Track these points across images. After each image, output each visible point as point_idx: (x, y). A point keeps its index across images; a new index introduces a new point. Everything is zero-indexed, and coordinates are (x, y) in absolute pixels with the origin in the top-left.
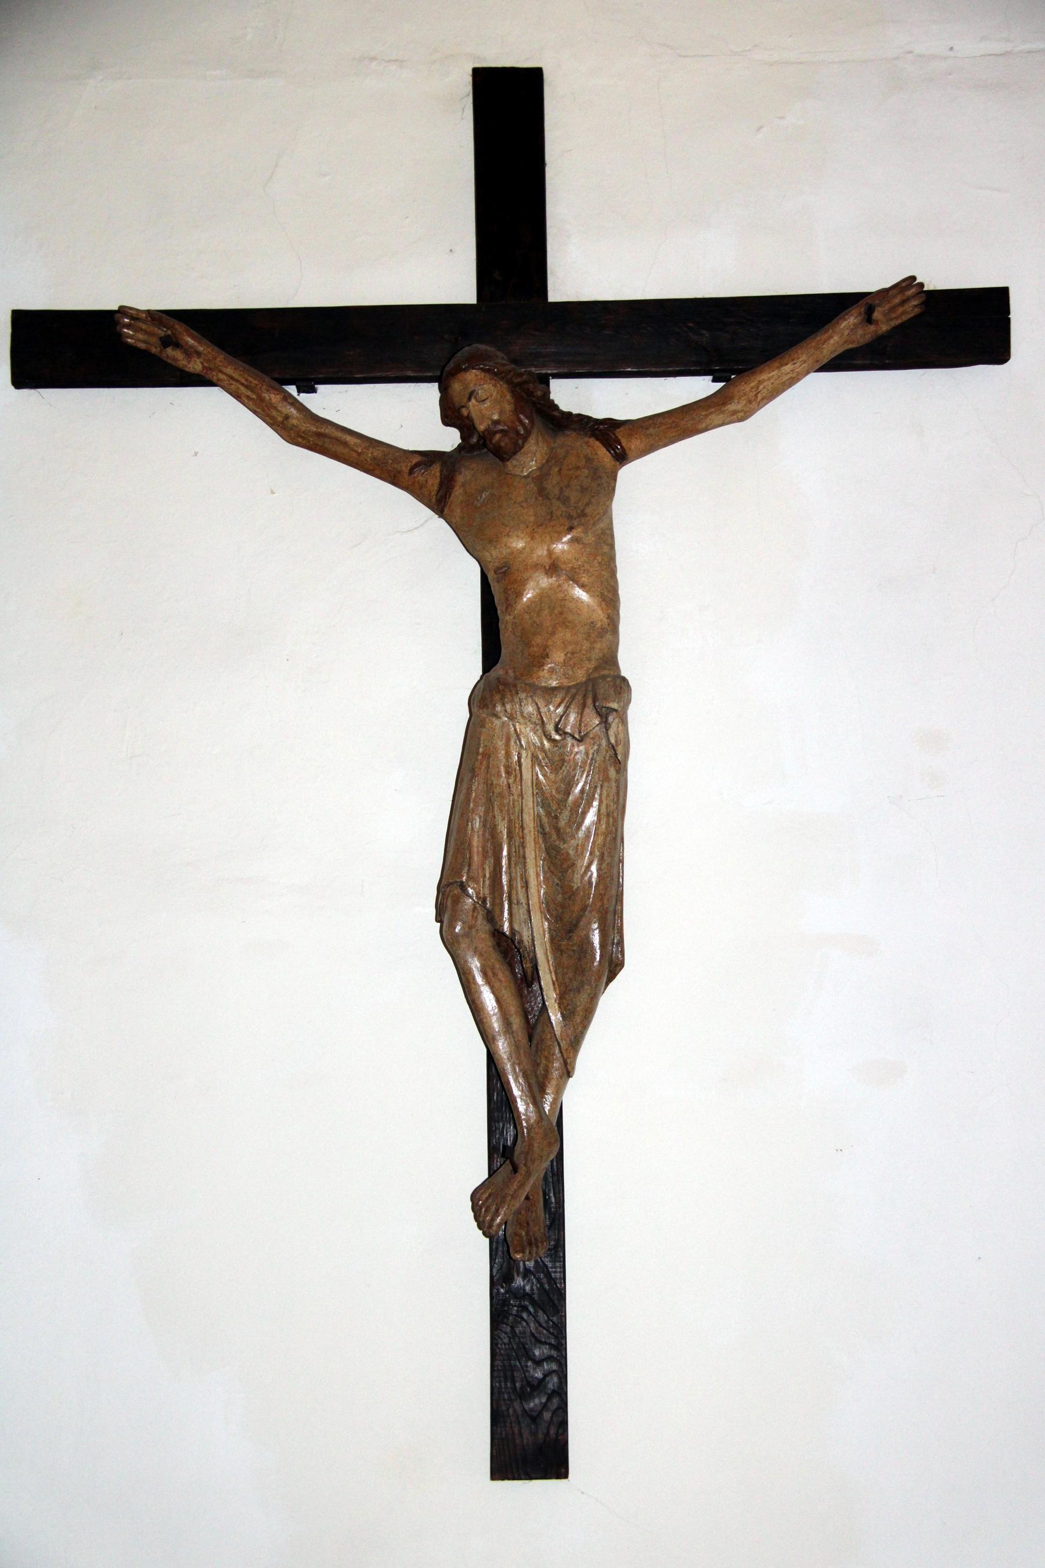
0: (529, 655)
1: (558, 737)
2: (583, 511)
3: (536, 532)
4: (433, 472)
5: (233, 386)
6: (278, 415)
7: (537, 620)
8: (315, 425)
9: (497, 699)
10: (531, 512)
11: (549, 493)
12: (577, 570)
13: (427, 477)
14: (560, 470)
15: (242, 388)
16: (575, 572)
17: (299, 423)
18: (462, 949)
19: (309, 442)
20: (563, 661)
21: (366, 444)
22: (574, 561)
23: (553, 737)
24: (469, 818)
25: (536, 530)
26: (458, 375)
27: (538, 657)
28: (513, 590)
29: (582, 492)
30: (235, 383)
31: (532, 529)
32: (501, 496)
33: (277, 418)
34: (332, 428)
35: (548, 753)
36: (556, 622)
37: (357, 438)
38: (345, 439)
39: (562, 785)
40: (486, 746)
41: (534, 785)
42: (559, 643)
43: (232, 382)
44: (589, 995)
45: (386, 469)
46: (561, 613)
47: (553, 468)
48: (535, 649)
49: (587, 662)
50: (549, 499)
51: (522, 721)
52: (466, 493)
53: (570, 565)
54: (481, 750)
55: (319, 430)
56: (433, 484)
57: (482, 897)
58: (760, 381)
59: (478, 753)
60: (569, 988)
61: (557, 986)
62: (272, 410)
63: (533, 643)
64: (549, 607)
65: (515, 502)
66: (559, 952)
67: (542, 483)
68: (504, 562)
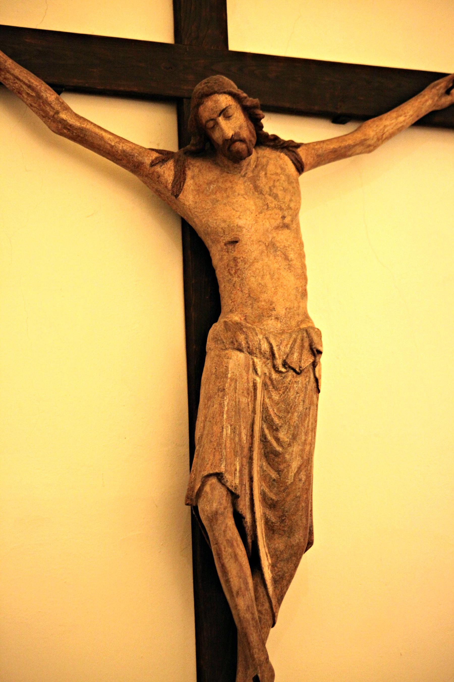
0: (259, 307)
1: (283, 370)
2: (289, 205)
3: (259, 218)
4: (169, 166)
5: (17, 85)
6: (51, 111)
7: (262, 282)
8: (79, 121)
9: (242, 338)
10: (252, 203)
11: (262, 190)
12: (287, 248)
13: (165, 169)
14: (266, 174)
15: (24, 87)
16: (286, 249)
17: (67, 118)
18: (218, 524)
19: (72, 134)
20: (284, 314)
21: (117, 140)
22: (285, 241)
23: (280, 370)
24: (223, 426)
25: (258, 216)
26: (212, 96)
27: (266, 309)
28: (242, 259)
29: (285, 192)
30: (18, 82)
31: (255, 215)
32: (227, 189)
33: (49, 113)
34: (91, 125)
35: (274, 382)
36: (277, 285)
37: (110, 134)
38: (102, 134)
39: (283, 406)
40: (233, 373)
41: (262, 405)
42: (281, 300)
43: (16, 81)
44: (294, 564)
45: (132, 160)
46: (279, 279)
47: (261, 172)
48: (263, 303)
49: (297, 316)
50: (263, 194)
51: (259, 355)
52: (196, 184)
53: (283, 244)
54: (229, 376)
55: (82, 125)
56: (169, 175)
57: (234, 486)
58: (385, 126)
59: (227, 377)
60: (280, 559)
61: (269, 557)
62: (47, 106)
63: (261, 299)
64: (270, 274)
65: (239, 194)
66: (272, 532)
67: (255, 182)
68: (234, 238)
